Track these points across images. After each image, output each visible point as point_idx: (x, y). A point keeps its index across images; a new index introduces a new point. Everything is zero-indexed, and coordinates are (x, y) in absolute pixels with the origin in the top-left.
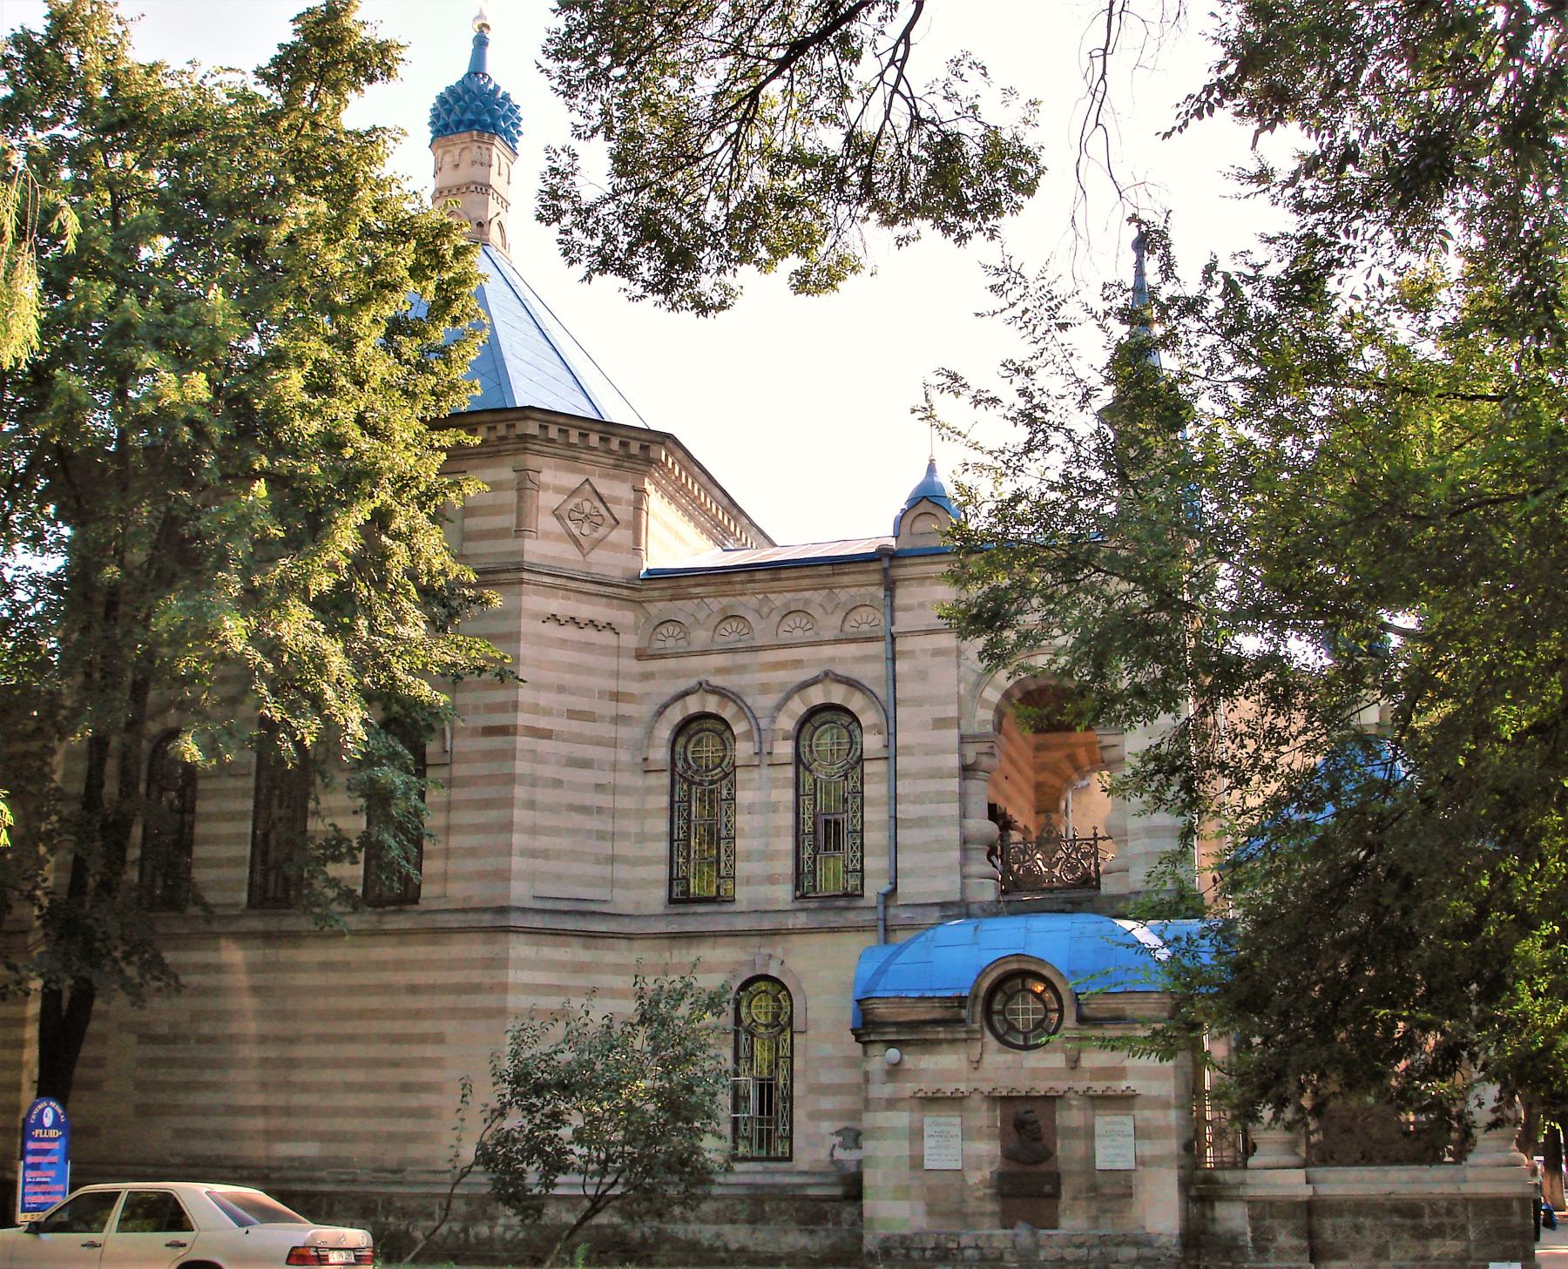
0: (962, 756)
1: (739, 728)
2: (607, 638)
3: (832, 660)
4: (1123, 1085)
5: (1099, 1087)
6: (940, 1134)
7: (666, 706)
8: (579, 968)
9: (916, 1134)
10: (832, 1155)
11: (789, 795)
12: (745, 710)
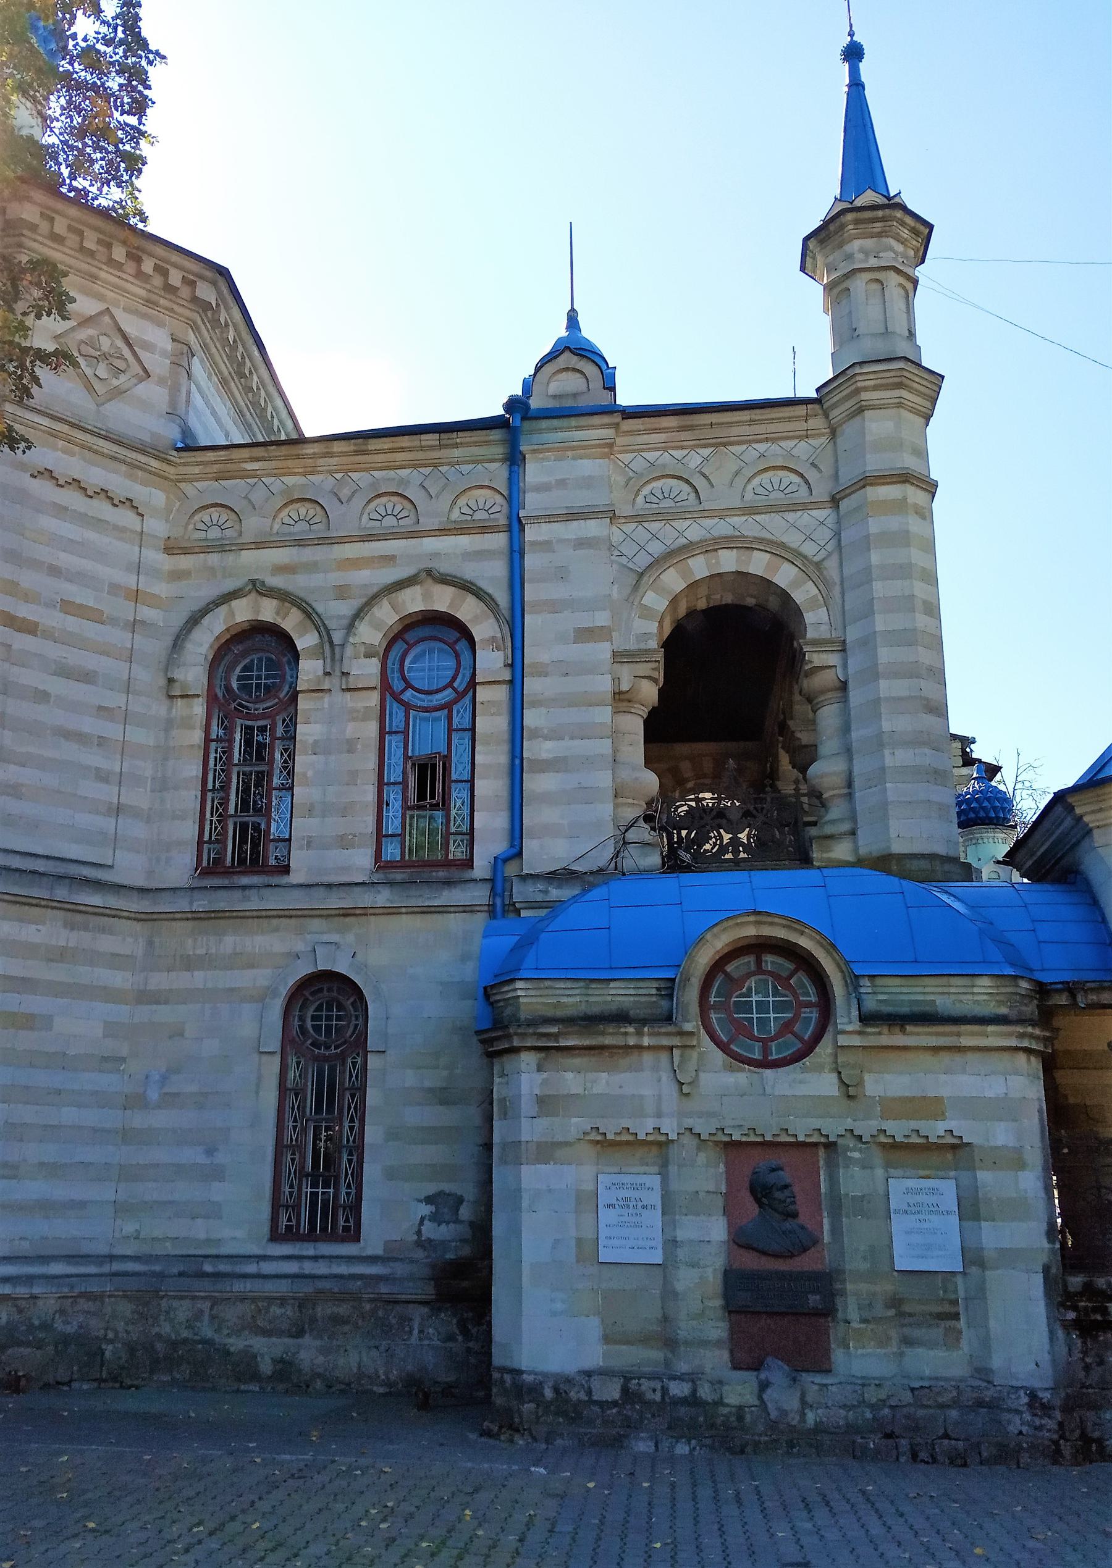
0: (616, 680)
1: (305, 641)
2: (126, 518)
3: (436, 555)
4: (940, 1127)
5: (898, 1129)
6: (625, 1204)
7: (205, 611)
8: (59, 955)
9: (587, 1201)
10: (419, 1233)
11: (371, 729)
12: (309, 614)
